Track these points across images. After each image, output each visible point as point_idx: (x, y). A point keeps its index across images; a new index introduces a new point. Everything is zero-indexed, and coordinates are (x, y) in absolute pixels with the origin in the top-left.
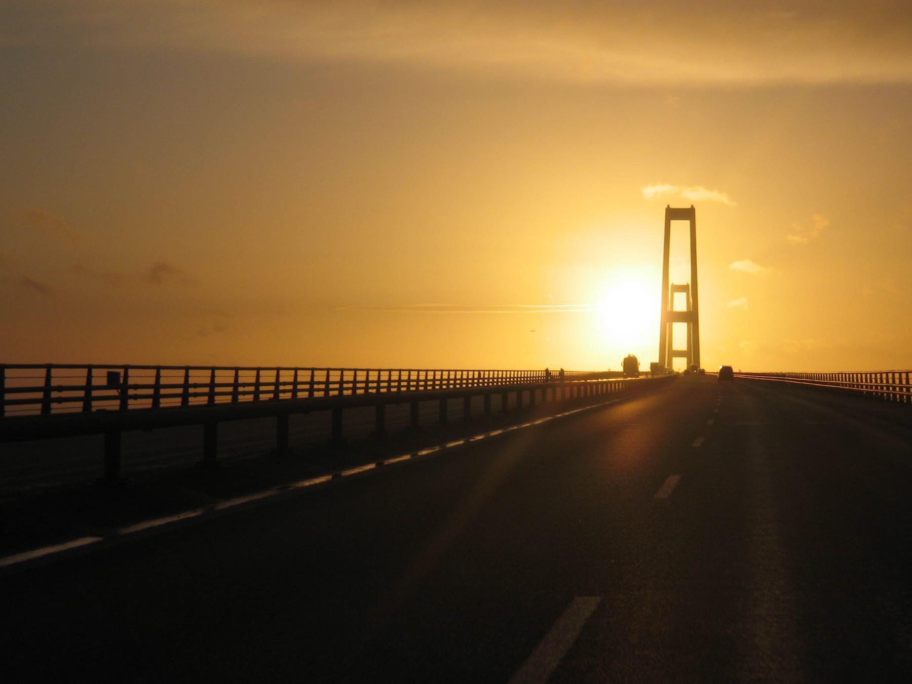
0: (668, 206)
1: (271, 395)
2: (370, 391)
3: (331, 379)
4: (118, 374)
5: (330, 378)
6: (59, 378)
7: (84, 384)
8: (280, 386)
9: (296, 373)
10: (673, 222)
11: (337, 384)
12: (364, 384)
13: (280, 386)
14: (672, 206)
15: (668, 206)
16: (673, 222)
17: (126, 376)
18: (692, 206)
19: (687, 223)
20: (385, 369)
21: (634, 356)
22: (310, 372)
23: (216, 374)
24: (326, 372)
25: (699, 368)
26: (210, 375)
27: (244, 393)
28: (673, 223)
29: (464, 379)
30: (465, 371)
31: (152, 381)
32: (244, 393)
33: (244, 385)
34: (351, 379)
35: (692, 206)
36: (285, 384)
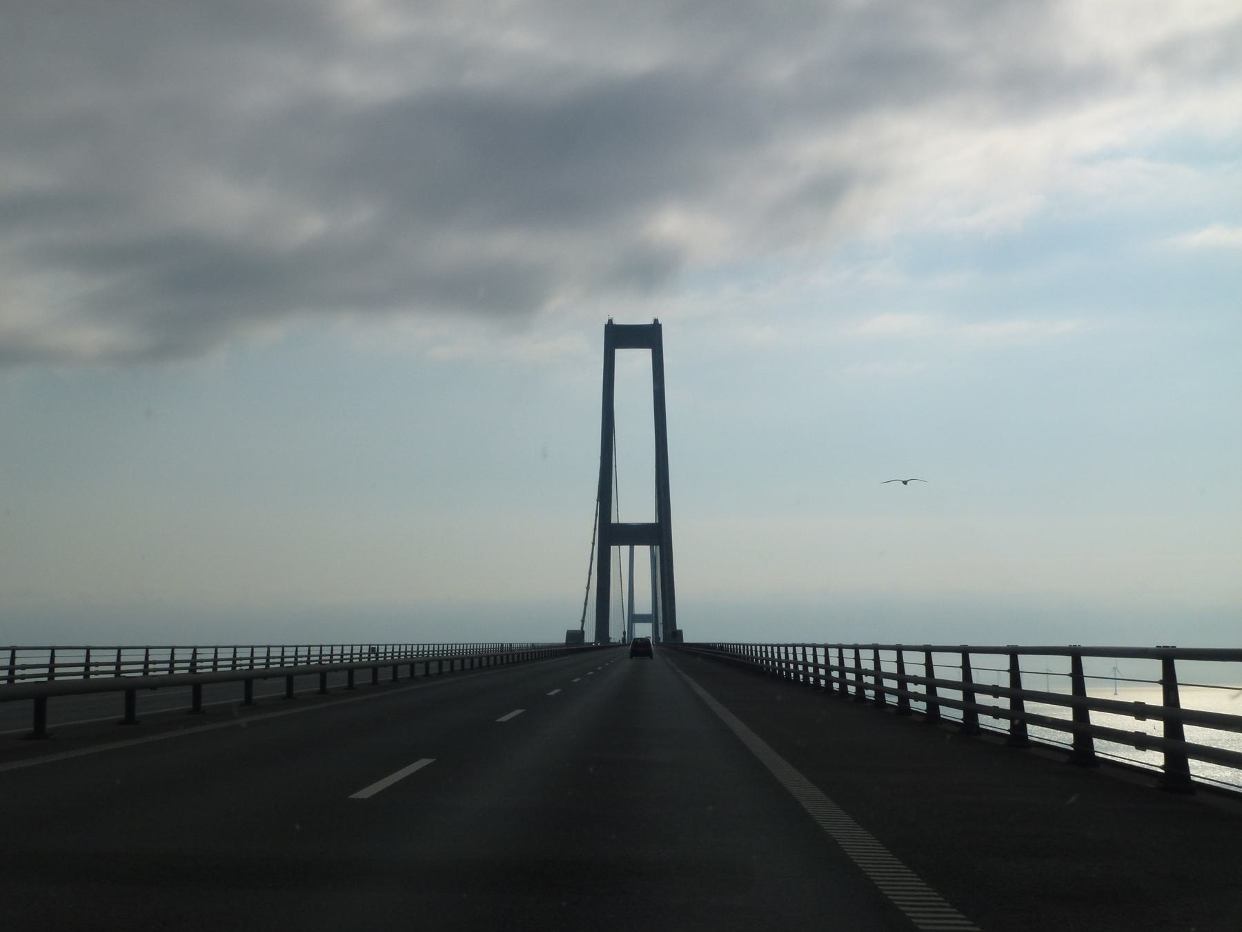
0: (610, 321)
1: (264, 667)
2: (388, 658)
3: (363, 651)
4: (375, 648)
5: (122, 658)
6: (96, 657)
7: (232, 657)
8: (56, 669)
9: (216, 651)
10: (619, 353)
11: (5, 669)
12: (143, 665)
13: (56, 669)
14: (616, 322)
15: (610, 321)
16: (619, 353)
17: (378, 649)
18: (656, 321)
19: (646, 355)
20: (128, 645)
21: (661, 325)
22: (84, 652)
23: (122, 654)
24: (50, 651)
25: (592, 643)
26: (50, 655)
27: (274, 663)
28: (620, 354)
29: (409, 652)
30: (769, 645)
31: (83, 660)
32: (274, 663)
33: (274, 658)
34: (340, 652)
35: (656, 321)
36: (302, 657)
